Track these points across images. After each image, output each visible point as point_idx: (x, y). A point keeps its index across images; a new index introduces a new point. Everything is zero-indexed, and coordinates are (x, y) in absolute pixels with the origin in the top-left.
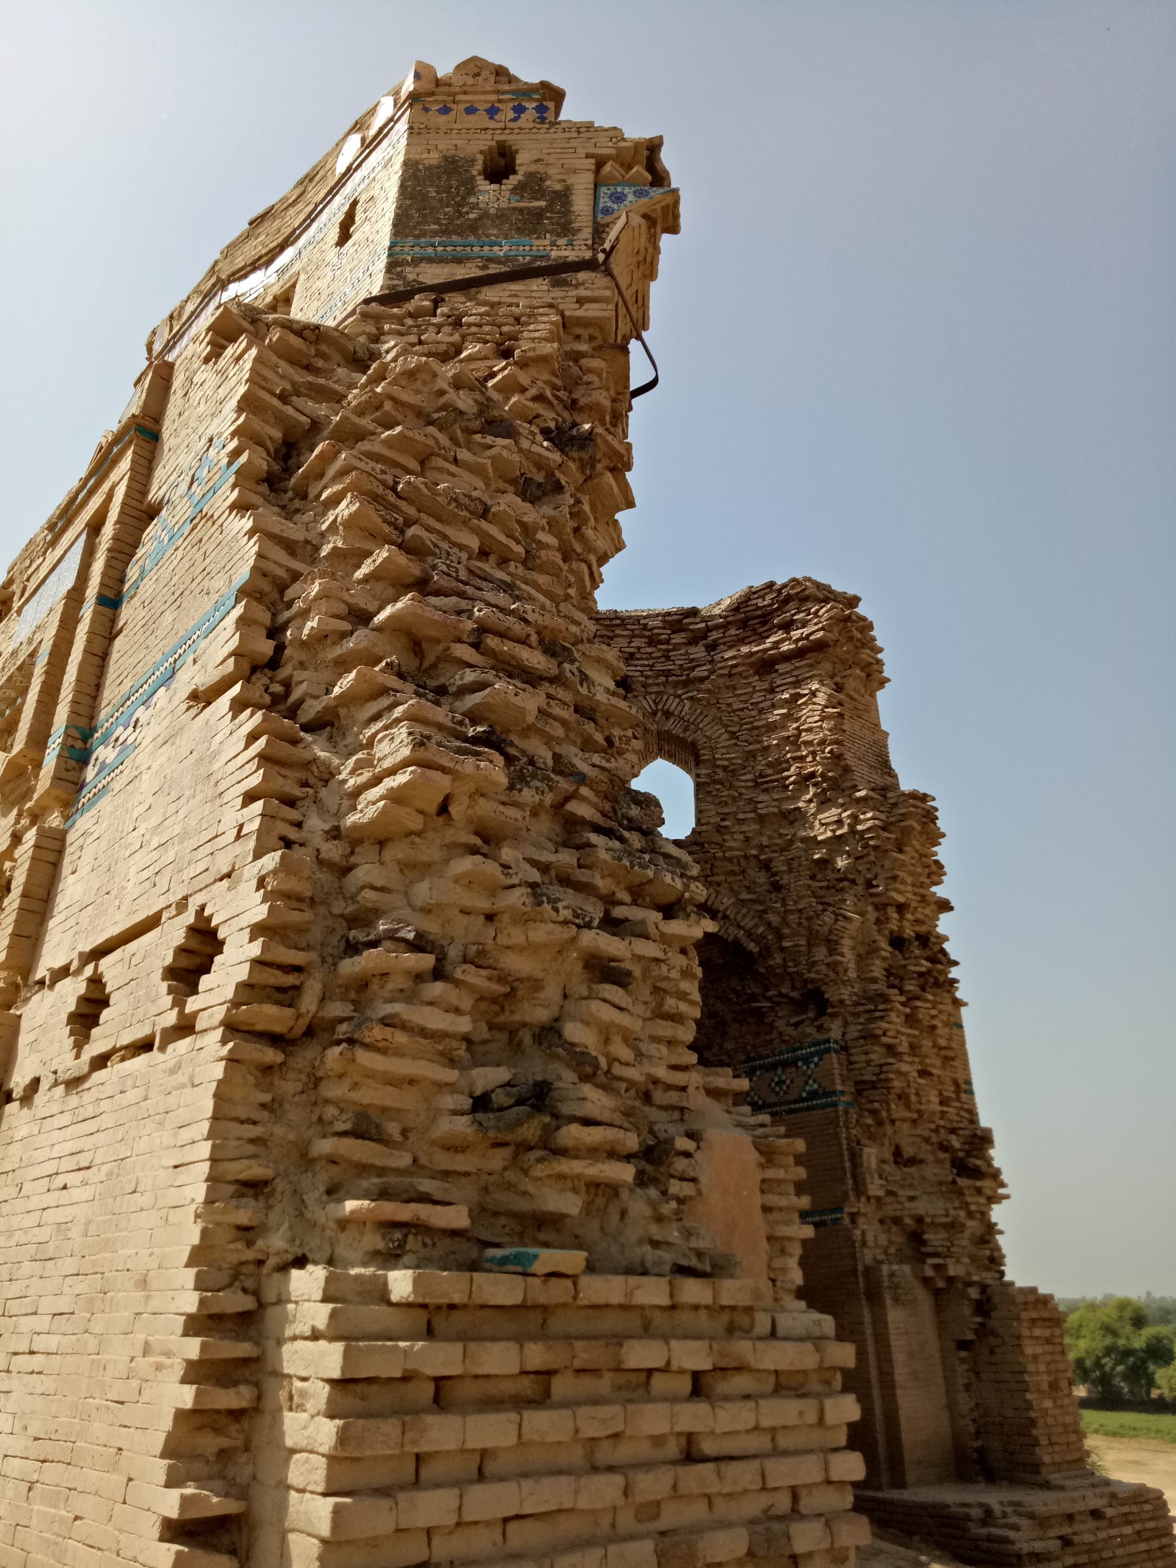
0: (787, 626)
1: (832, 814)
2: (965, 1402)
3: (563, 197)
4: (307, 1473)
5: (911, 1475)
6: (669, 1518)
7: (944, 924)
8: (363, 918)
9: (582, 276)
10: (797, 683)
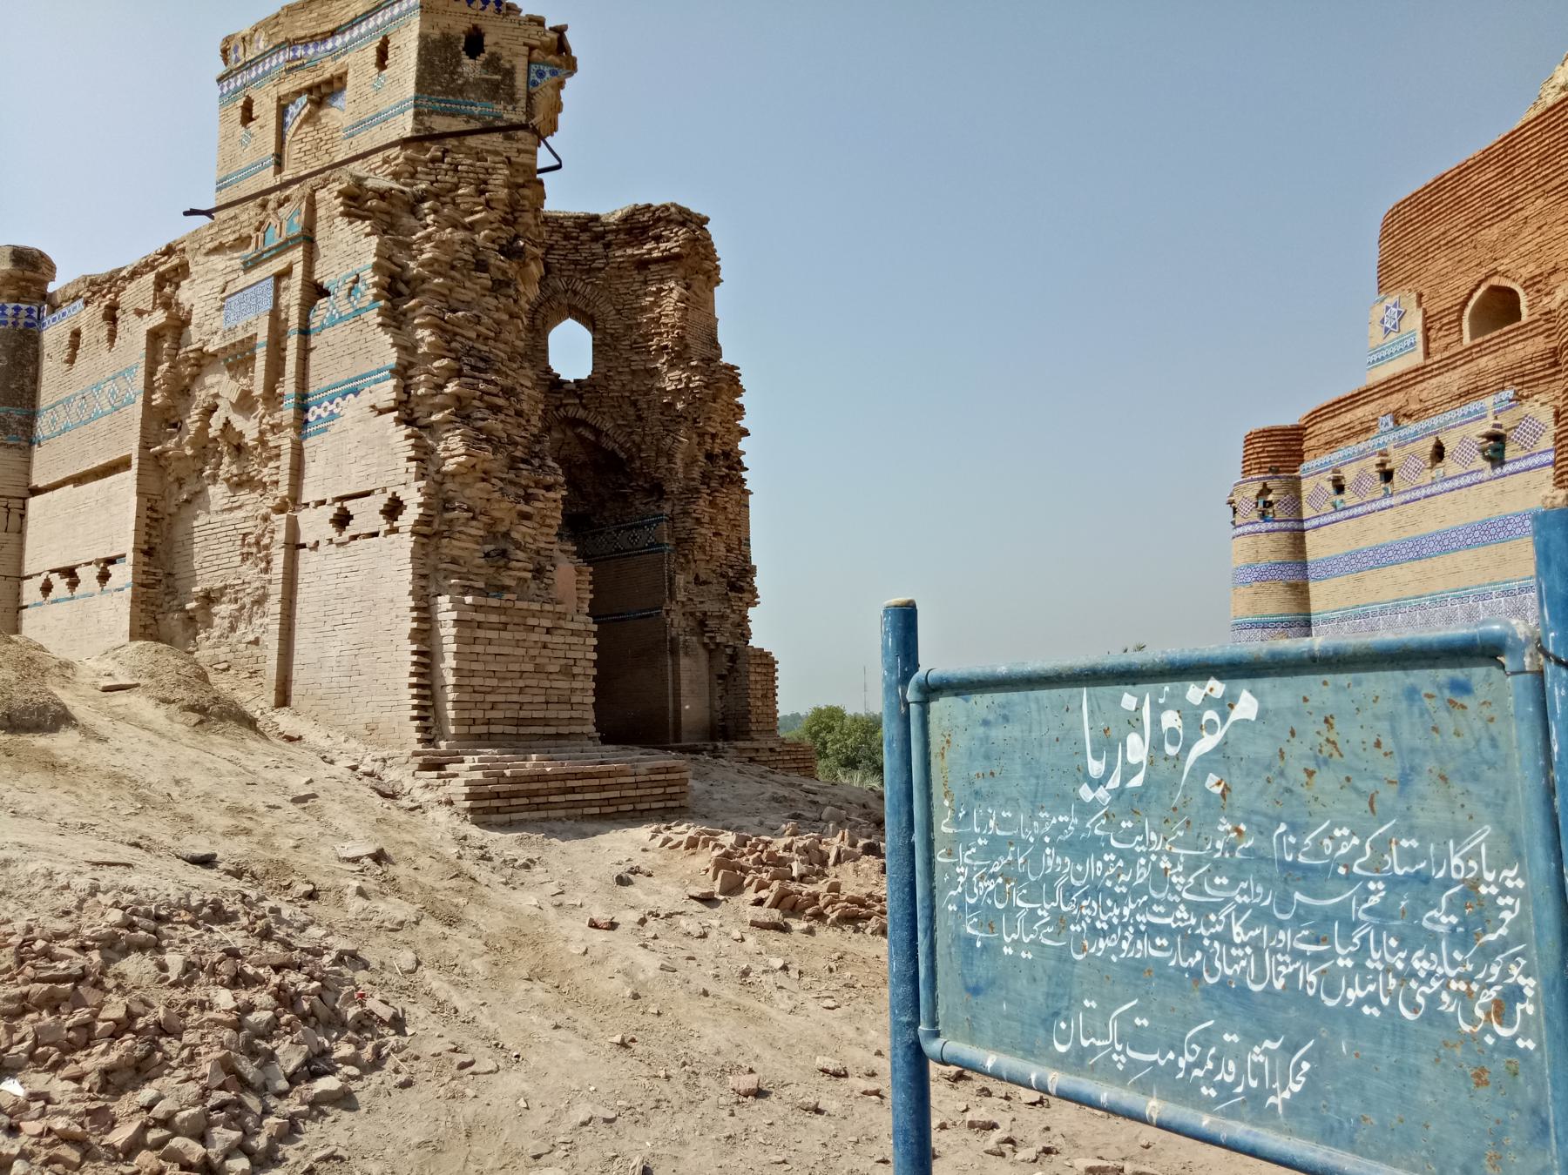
0: (658, 239)
1: (675, 374)
2: (718, 704)
3: (509, 73)
5: (684, 735)
6: (538, 661)
7: (743, 444)
8: (448, 500)
9: (521, 134)
10: (662, 281)
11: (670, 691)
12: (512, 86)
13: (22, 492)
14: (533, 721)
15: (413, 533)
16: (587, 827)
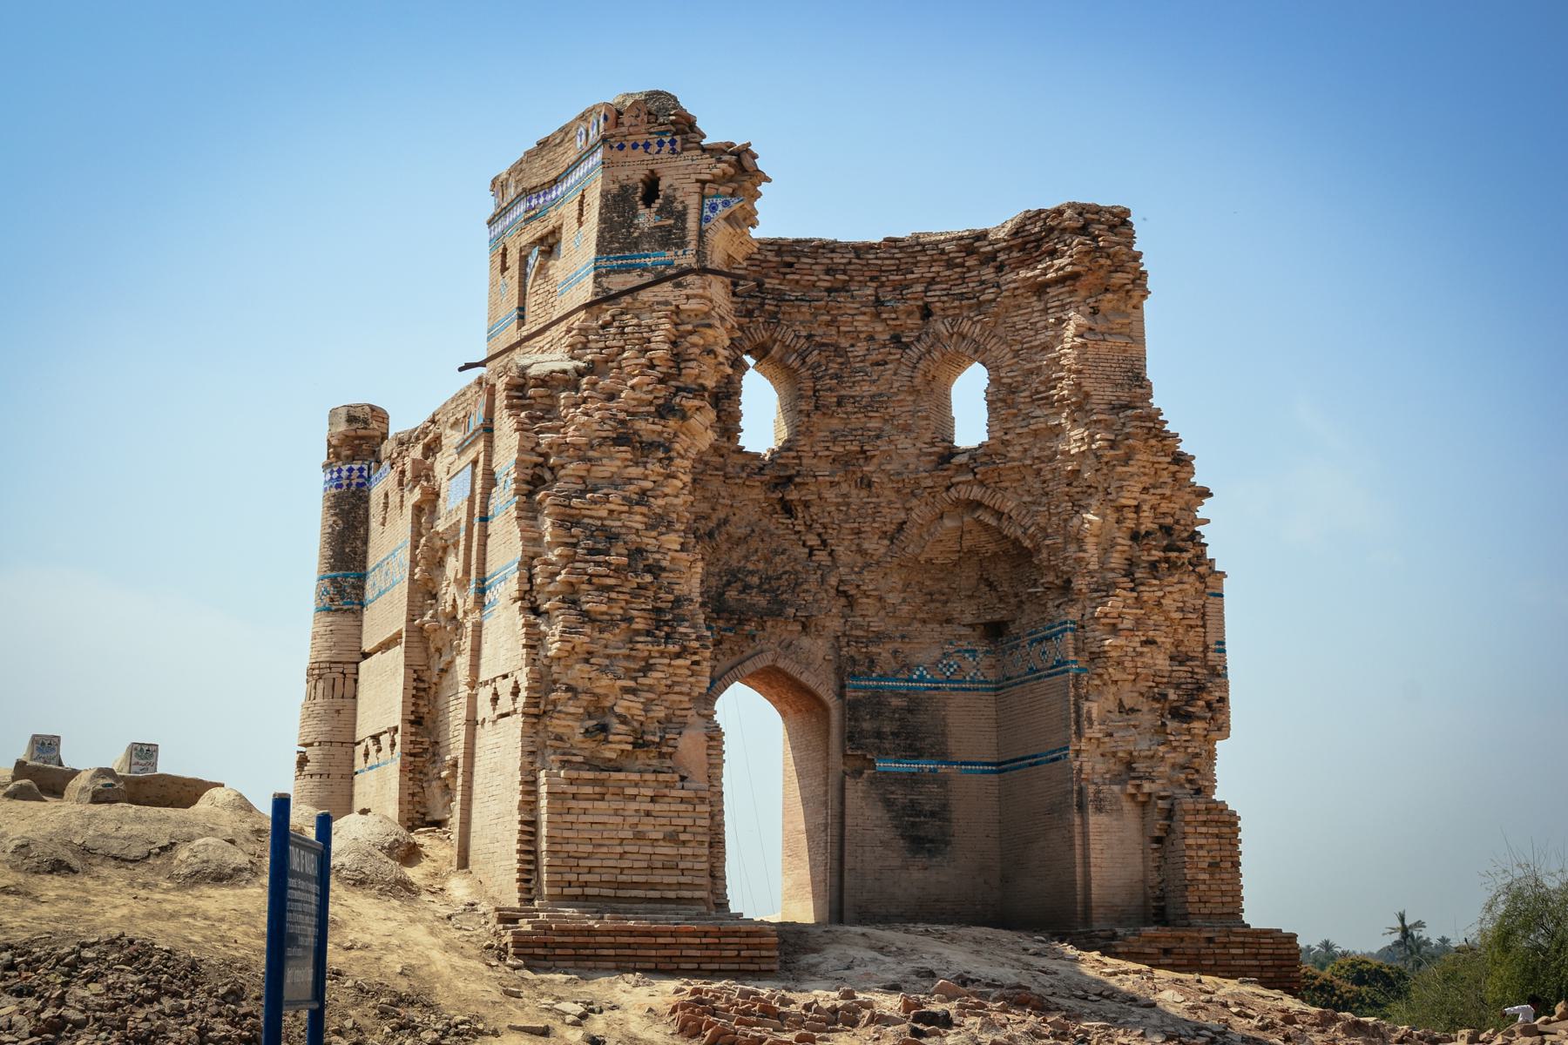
0: (1053, 254)
3: (682, 216)
4: (544, 811)
6: (640, 828)
9: (690, 278)
11: (1078, 859)
12: (684, 229)
13: (356, 657)
14: (635, 885)
15: (524, 714)
16: (589, 975)
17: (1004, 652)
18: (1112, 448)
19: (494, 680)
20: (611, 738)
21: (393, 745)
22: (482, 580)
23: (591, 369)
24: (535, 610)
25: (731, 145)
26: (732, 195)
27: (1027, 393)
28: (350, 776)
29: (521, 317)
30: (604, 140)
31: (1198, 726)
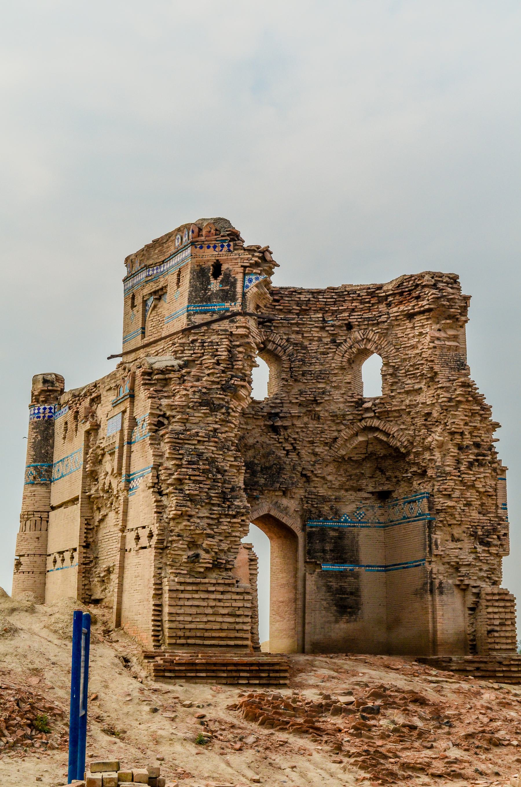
0: (418, 298)
3: (233, 285)
9: (238, 318)
11: (430, 620)
12: (235, 292)
13: (48, 508)
15: (155, 548)
17: (389, 507)
18: (449, 402)
19: (137, 529)
20: (201, 561)
21: (72, 558)
22: (128, 475)
23: (187, 364)
24: (160, 493)
25: (259, 247)
26: (260, 274)
27: (403, 371)
28: (44, 573)
29: (143, 333)
30: (193, 244)
31: (493, 550)
